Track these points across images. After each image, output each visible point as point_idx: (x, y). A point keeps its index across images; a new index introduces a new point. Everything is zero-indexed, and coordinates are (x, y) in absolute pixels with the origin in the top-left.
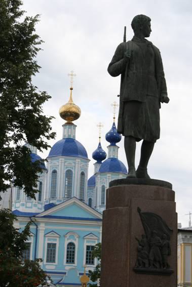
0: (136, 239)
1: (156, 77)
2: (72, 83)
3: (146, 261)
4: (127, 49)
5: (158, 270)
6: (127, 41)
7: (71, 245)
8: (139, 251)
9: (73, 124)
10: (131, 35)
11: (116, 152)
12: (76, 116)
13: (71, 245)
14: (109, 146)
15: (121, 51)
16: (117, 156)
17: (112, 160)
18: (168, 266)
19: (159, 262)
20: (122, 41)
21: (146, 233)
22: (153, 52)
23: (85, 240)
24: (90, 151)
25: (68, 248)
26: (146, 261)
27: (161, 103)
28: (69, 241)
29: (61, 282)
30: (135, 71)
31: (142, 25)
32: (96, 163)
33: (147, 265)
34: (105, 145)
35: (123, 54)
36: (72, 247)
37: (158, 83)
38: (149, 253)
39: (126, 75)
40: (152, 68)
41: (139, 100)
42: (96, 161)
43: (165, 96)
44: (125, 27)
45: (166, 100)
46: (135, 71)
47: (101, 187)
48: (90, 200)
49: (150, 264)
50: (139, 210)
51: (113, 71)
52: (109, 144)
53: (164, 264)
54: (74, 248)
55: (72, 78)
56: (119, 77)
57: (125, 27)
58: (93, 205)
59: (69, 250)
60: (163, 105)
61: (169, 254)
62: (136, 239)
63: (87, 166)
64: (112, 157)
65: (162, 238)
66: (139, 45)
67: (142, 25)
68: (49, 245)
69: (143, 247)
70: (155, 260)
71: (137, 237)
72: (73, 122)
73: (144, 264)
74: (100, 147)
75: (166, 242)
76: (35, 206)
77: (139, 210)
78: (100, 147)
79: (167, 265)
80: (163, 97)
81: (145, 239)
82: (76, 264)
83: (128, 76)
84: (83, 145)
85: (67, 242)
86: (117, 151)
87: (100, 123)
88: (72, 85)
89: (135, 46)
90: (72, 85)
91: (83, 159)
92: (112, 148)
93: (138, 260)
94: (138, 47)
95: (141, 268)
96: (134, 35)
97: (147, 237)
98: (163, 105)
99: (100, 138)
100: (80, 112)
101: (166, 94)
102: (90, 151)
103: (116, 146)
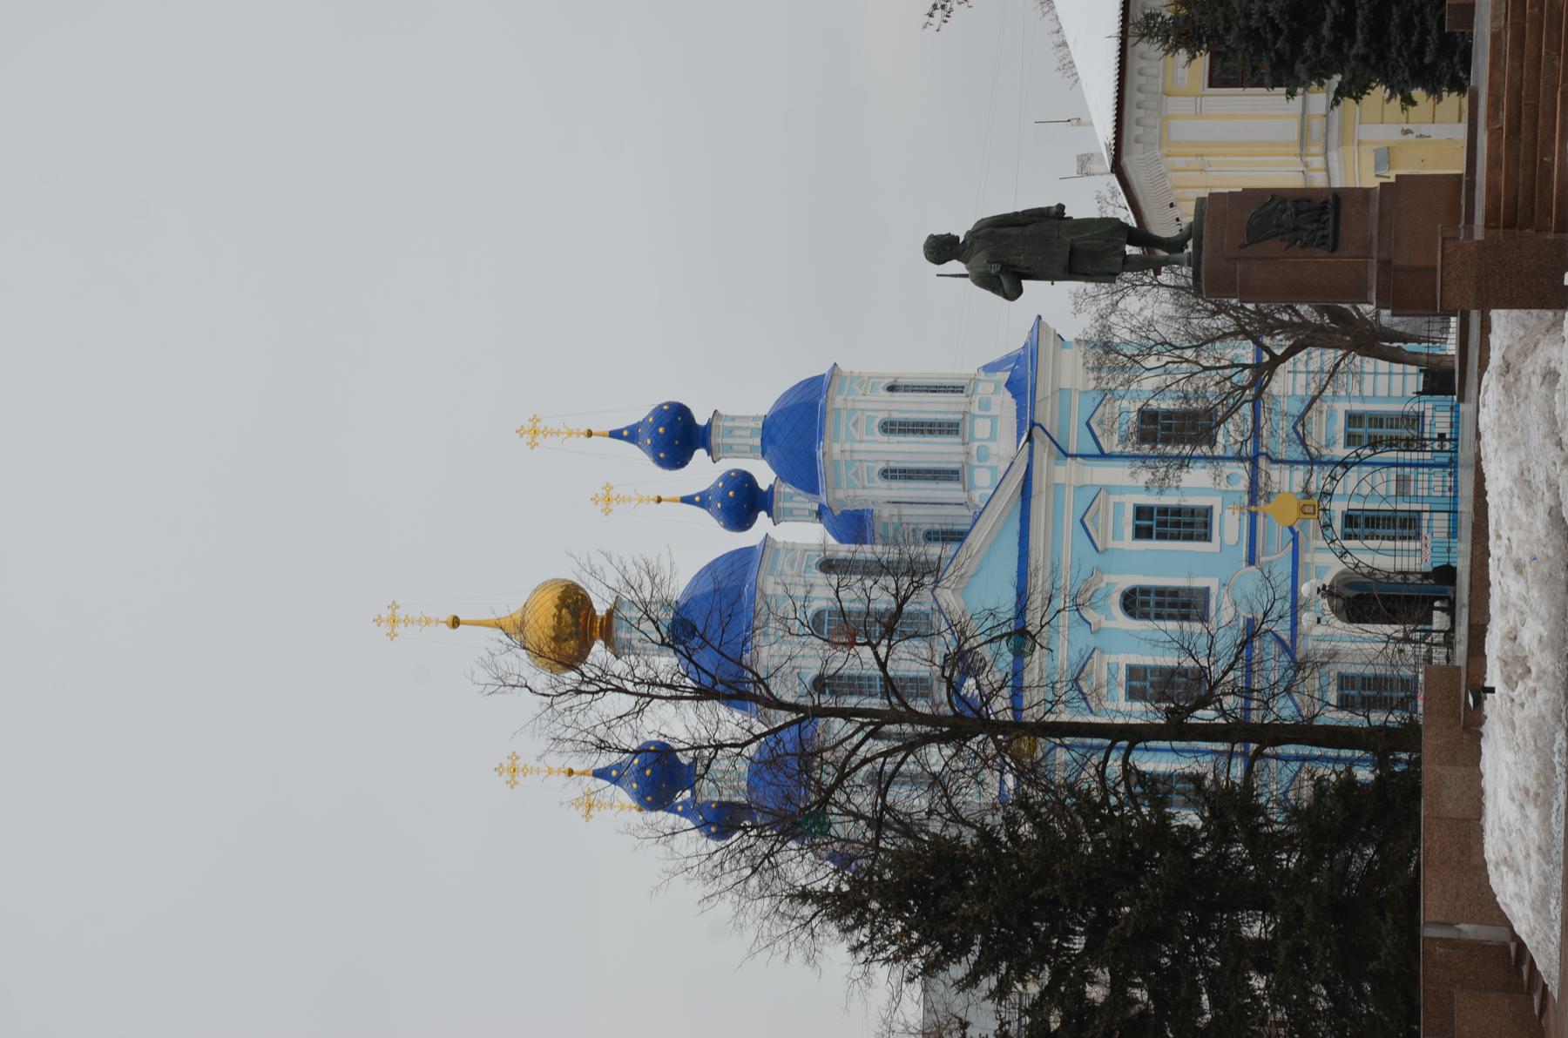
0: (1287, 249)
1: (1025, 225)
2: (428, 622)
3: (1320, 234)
4: (982, 270)
5: (1331, 216)
6: (966, 272)
7: (1134, 602)
8: (1304, 246)
9: (610, 613)
10: (956, 266)
11: (736, 424)
12: (573, 601)
13: (1134, 602)
14: (710, 452)
15: (987, 281)
16: (755, 418)
17: (772, 441)
18: (1326, 202)
19: (1320, 215)
20: (968, 280)
21: (1277, 235)
22: (987, 230)
23: (1111, 544)
24: (713, 540)
25: (1146, 616)
26: (1320, 234)
27: (961, 241)
28: (1117, 611)
29: (1286, 636)
30: (1022, 257)
31: (941, 249)
32: (770, 514)
33: (1326, 232)
34: (702, 471)
35: (991, 276)
36: (1139, 598)
37: (1034, 222)
38: (1306, 230)
39: (1025, 271)
40: (1014, 231)
41: (1068, 249)
42: (762, 515)
43: (1054, 210)
44: (938, 275)
45: (1061, 207)
46: (1022, 257)
47: (885, 438)
48: (932, 536)
49: (1323, 229)
50: (1243, 246)
51: (1014, 293)
52: (700, 454)
53: (1323, 208)
54: (1145, 591)
55: (408, 621)
56: (1025, 283)
57: (938, 275)
58: (958, 518)
59: (1152, 610)
60: (1068, 213)
61: (1309, 201)
62: (1287, 249)
63: (791, 548)
64: (757, 441)
65: (1284, 211)
66: (979, 251)
67: (941, 249)
68: (1141, 533)
69: (1298, 239)
70: (1317, 221)
71: (1284, 247)
72: (601, 609)
73: (1323, 237)
74: (699, 500)
75: (1289, 204)
76: (985, 405)
77: (1243, 246)
78: (699, 500)
79: (1323, 203)
80: (1057, 213)
81: (1286, 237)
82: (1213, 583)
83: (1027, 268)
84: (725, 552)
85: (1123, 622)
86: (733, 419)
87: (608, 488)
88: (438, 622)
89: (980, 259)
90: (438, 622)
91: (764, 565)
92: (715, 440)
93: (1317, 246)
94: (980, 254)
95: (1329, 241)
96: (955, 261)
97: (1284, 233)
98: (1068, 213)
99: (659, 500)
100: (555, 581)
101: (1049, 208)
102: (713, 540)
103: (709, 424)
